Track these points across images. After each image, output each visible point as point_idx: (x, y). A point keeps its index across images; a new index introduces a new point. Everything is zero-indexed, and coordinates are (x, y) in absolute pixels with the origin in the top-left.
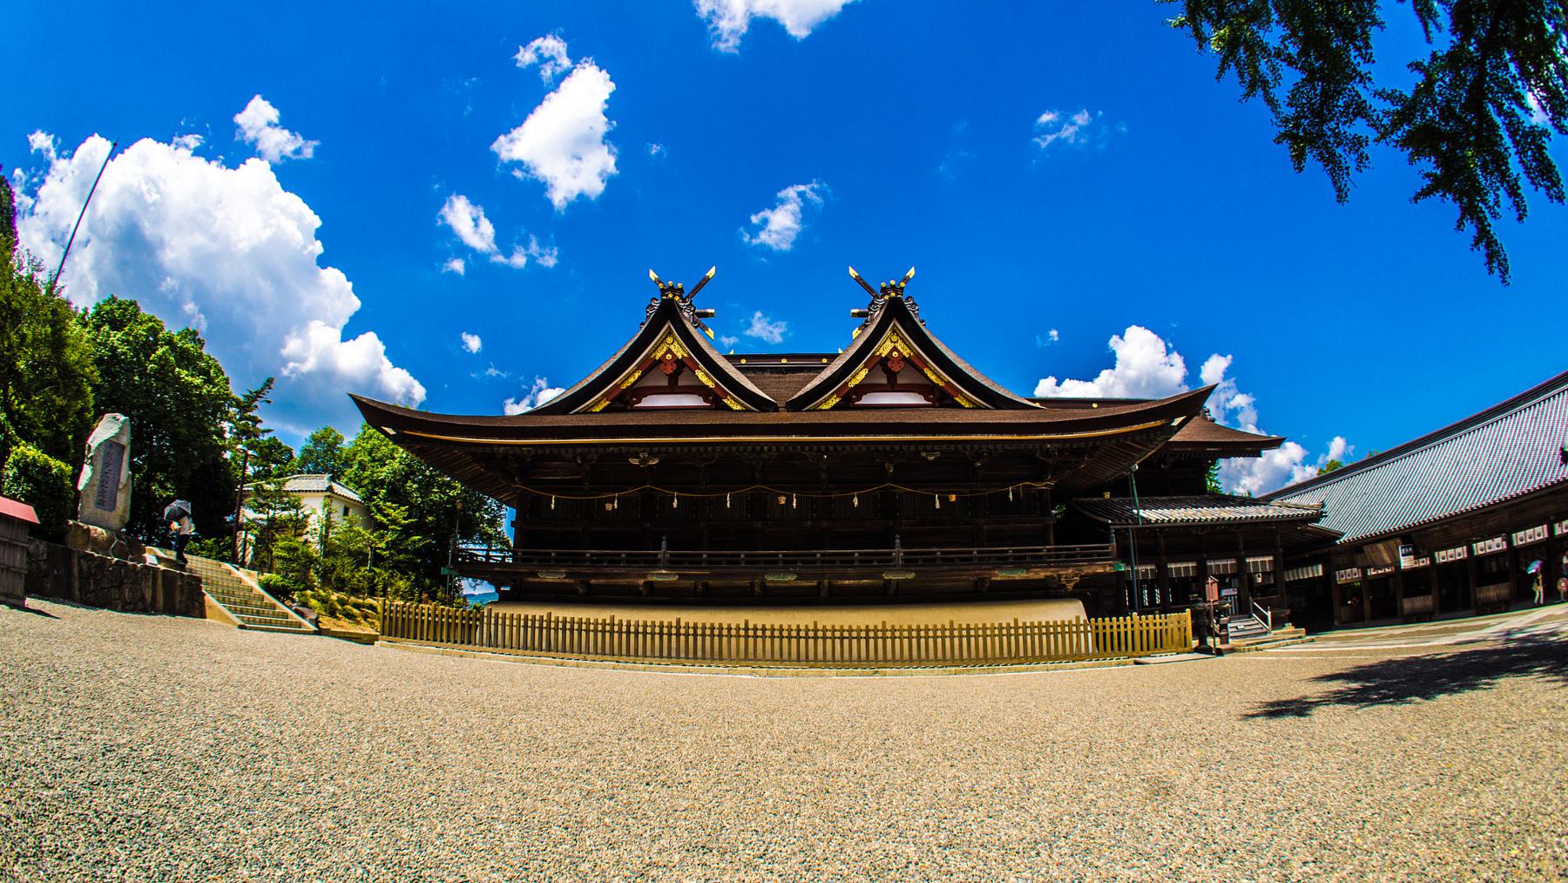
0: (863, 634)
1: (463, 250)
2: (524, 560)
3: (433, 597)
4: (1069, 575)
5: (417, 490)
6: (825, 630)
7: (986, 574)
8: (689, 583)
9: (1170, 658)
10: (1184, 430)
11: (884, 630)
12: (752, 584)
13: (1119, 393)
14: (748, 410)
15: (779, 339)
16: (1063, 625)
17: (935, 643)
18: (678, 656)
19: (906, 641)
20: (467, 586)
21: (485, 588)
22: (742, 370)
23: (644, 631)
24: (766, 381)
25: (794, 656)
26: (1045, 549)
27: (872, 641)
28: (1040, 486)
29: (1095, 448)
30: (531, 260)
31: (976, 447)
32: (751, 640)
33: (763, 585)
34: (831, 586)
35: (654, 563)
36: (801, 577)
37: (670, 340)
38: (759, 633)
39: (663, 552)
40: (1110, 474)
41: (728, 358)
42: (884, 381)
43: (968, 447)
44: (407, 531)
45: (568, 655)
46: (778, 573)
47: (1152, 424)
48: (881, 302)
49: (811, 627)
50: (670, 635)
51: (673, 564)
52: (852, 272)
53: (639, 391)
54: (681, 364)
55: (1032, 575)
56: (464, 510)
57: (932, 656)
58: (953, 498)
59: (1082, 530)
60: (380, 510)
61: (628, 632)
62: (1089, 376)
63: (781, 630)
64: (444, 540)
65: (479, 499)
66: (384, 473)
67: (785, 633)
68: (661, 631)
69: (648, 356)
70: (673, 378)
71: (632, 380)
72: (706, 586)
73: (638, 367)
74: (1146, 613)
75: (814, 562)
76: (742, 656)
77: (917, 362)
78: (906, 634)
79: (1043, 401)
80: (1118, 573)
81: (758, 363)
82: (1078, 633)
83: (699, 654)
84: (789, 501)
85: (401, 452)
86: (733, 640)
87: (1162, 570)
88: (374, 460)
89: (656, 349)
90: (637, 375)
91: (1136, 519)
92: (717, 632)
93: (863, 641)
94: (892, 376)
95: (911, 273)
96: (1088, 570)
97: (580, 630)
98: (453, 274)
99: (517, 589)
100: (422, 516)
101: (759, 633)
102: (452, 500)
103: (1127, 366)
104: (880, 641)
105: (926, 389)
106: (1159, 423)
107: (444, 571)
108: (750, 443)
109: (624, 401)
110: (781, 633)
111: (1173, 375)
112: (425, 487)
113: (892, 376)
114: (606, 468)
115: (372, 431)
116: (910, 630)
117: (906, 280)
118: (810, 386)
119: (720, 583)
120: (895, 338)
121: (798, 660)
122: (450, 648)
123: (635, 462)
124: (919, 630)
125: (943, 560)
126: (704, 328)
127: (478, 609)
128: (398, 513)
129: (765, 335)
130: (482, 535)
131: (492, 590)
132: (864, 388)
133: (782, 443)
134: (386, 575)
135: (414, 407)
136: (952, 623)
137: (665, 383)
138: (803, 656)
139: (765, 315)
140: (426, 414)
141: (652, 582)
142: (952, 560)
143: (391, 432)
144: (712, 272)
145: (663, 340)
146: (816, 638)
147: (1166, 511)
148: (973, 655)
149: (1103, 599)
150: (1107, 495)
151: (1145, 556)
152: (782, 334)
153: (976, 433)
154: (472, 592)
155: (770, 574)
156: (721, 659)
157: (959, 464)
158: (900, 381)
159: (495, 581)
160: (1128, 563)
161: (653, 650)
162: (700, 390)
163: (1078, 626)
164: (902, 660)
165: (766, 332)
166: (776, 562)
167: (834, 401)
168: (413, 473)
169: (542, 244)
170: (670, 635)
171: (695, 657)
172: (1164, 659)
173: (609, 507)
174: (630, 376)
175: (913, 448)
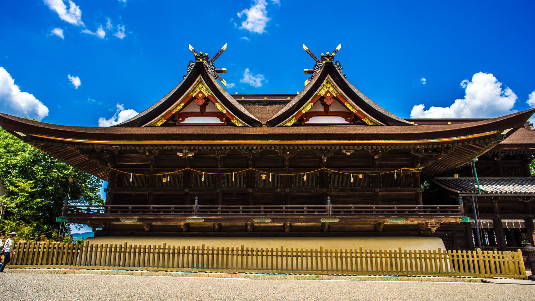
0: (309, 254)
1: (62, 24)
2: (112, 212)
3: (49, 236)
5: (42, 170)
6: (287, 251)
7: (381, 221)
8: (210, 224)
9: (508, 281)
10: (512, 136)
11: (321, 252)
12: (246, 224)
13: (467, 114)
14: (245, 126)
15: (259, 85)
17: (351, 260)
18: (203, 267)
19: (334, 259)
20: (74, 229)
21: (86, 230)
22: (242, 103)
23: (183, 252)
24: (256, 110)
25: (270, 267)
26: (416, 207)
27: (314, 259)
28: (414, 170)
29: (448, 148)
30: (109, 34)
31: (374, 147)
32: (245, 257)
34: (291, 226)
35: (190, 212)
36: (274, 220)
37: (201, 86)
38: (250, 253)
39: (196, 206)
40: (459, 163)
41: (234, 96)
42: (322, 110)
44: (32, 196)
45: (136, 268)
46: (261, 218)
47: (487, 133)
48: (321, 64)
49: (279, 250)
50: (198, 254)
51: (201, 212)
52: (305, 47)
54: (207, 100)
55: (409, 222)
56: (74, 182)
59: (439, 197)
60: (12, 183)
62: (447, 103)
63: (262, 251)
64: (59, 200)
65: (85, 176)
66: (16, 160)
67: (265, 253)
68: (193, 252)
70: (203, 107)
71: (179, 108)
72: (220, 225)
73: (183, 101)
74: (487, 249)
76: (240, 266)
77: (341, 99)
79: (416, 121)
80: (465, 223)
82: (440, 259)
83: (215, 265)
84: (267, 177)
85: (30, 148)
86: (235, 257)
87: (497, 224)
88: (8, 152)
89: (192, 91)
90: (182, 105)
91: (477, 191)
92: (226, 253)
93: (309, 258)
95: (339, 47)
96: (445, 220)
97: (144, 253)
98: (56, 37)
99: (106, 229)
100: (45, 186)
101: (250, 253)
102: (66, 177)
103: (474, 98)
104: (319, 259)
105: (347, 114)
106: (492, 133)
107: (58, 220)
108: (245, 144)
109: (174, 120)
110: (261, 253)
111: (508, 103)
112: (48, 169)
114: (164, 158)
115: (7, 134)
116: (337, 252)
117: (336, 51)
118: (280, 113)
120: (328, 85)
121: (272, 269)
122: (57, 269)
123: (180, 154)
124: (342, 253)
125: (356, 212)
126: (221, 79)
127: (80, 242)
128: (27, 185)
129: (251, 82)
131: (90, 230)
133: (264, 145)
134: (14, 224)
135: (39, 120)
136: (361, 249)
137: (198, 110)
138: (275, 267)
140: (48, 125)
141: (188, 224)
142: (361, 212)
143: (22, 135)
144: (225, 47)
145: (197, 86)
146: (282, 256)
147: (499, 187)
148: (374, 269)
149: (456, 239)
150: (456, 176)
151: (484, 213)
152: (262, 82)
153: (375, 139)
154: (77, 232)
156: (227, 268)
157: (363, 157)
158: (331, 110)
159: (93, 226)
160: (472, 217)
161: (188, 264)
162: (218, 115)
163: (440, 254)
164: (332, 270)
165: (253, 81)
166: (260, 212)
167: (293, 121)
168: (39, 160)
169: (115, 22)
170: (198, 254)
171: (212, 268)
172: (503, 281)
173: (164, 180)
174: (177, 107)
175: (338, 148)
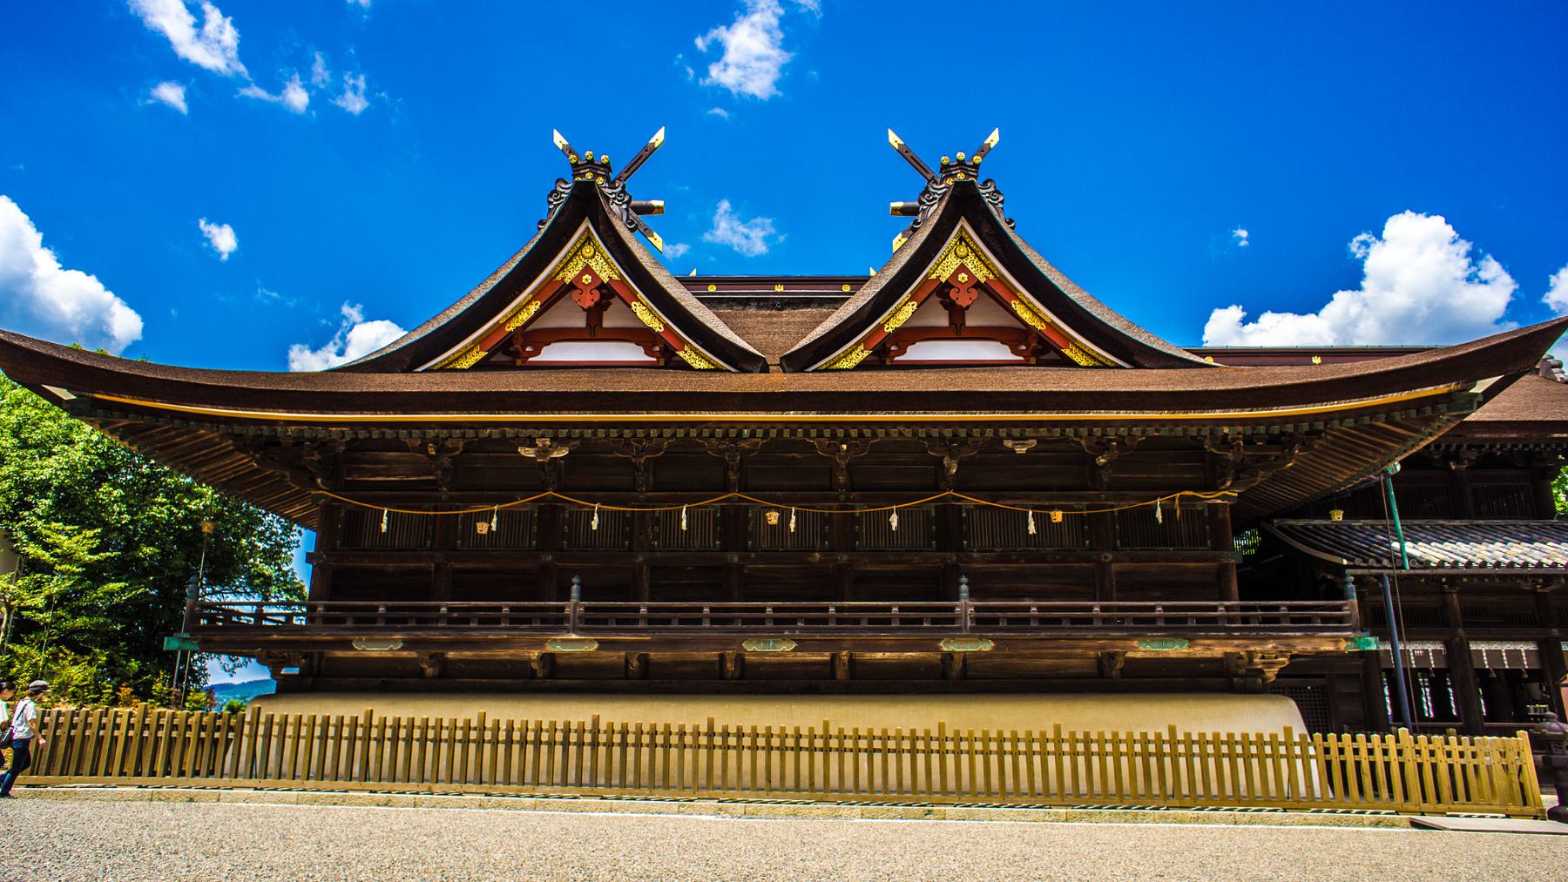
0: (906, 745)
1: (182, 71)
2: (328, 620)
3: (144, 693)
4: (1270, 653)
5: (123, 499)
6: (842, 737)
7: (1118, 646)
8: (616, 656)
9: (1488, 823)
10: (1500, 400)
11: (942, 739)
12: (722, 657)
13: (1368, 335)
14: (718, 370)
15: (760, 248)
16: (1260, 742)
17: (1030, 763)
19: (979, 759)
20: (217, 671)
21: (251, 673)
22: (709, 302)
23: (535, 739)
24: (750, 322)
25: (790, 782)
26: (1221, 607)
27: (921, 758)
28: (1213, 498)
29: (1314, 433)
30: (319, 100)
32: (718, 753)
33: (740, 659)
34: (852, 661)
35: (557, 622)
36: (802, 645)
37: (588, 251)
38: (732, 741)
39: (574, 605)
40: (1344, 478)
41: (686, 282)
42: (943, 321)
43: (1084, 431)
44: (94, 574)
45: (398, 785)
46: (765, 640)
47: (1429, 391)
48: (940, 189)
49: (819, 731)
50: (580, 744)
51: (590, 622)
52: (894, 139)
53: (537, 336)
54: (607, 293)
55: (1199, 651)
56: (217, 534)
57: (1024, 786)
58: (1057, 516)
59: (1288, 577)
60: (34, 537)
61: (509, 742)
62: (1312, 304)
64: (172, 585)
65: (248, 514)
66: (47, 469)
68: (567, 738)
69: (551, 278)
70: (595, 313)
71: (524, 317)
72: (644, 660)
73: (535, 296)
74: (1429, 731)
75: (825, 621)
78: (979, 746)
79: (1219, 354)
80: (1363, 654)
81: (742, 291)
83: (630, 778)
84: (784, 520)
85: (87, 432)
86: (688, 753)
87: (1457, 655)
88: (25, 445)
89: (564, 266)
90: (533, 308)
91: (1397, 559)
92: (660, 740)
93: (906, 757)
94: (956, 313)
95: (994, 138)
96: (1305, 645)
97: (423, 741)
98: (163, 109)
99: (310, 670)
100: (131, 546)
101: (732, 741)
102: (193, 518)
103: (1388, 286)
104: (935, 758)
105: (1016, 335)
107: (170, 644)
108: (719, 423)
109: (509, 353)
110: (766, 742)
111: (1489, 300)
112: (140, 494)
113: (956, 313)
114: (480, 464)
115: (21, 392)
116: (986, 739)
117: (984, 151)
118: (820, 331)
119: (667, 655)
120: (962, 250)
121: (797, 788)
123: (529, 453)
124: (1001, 740)
125: (1042, 620)
126: (647, 233)
127: (234, 710)
128: (79, 543)
130: (250, 579)
131: (263, 674)
132: (909, 335)
133: (773, 424)
136: (1057, 729)
137: (580, 322)
139: (735, 206)
141: (552, 656)
142: (1058, 621)
143: (65, 394)
144: (659, 137)
145: (577, 252)
146: (826, 750)
147: (1462, 547)
148: (1097, 787)
149: (1337, 699)
150: (1338, 516)
151: (1419, 623)
152: (767, 240)
153: (1098, 408)
154: (226, 679)
155: (750, 640)
156: (666, 786)
157: (1065, 460)
158: (971, 321)
159: (272, 660)
160: (1385, 636)
161: (550, 772)
162: (641, 336)
163: (1289, 744)
164: (973, 792)
165: (742, 237)
166: (762, 621)
168: (114, 470)
169: (338, 65)
170: (580, 744)
171: (623, 784)
172: (1475, 823)
173: (482, 528)
174: (520, 312)
175: (989, 433)
